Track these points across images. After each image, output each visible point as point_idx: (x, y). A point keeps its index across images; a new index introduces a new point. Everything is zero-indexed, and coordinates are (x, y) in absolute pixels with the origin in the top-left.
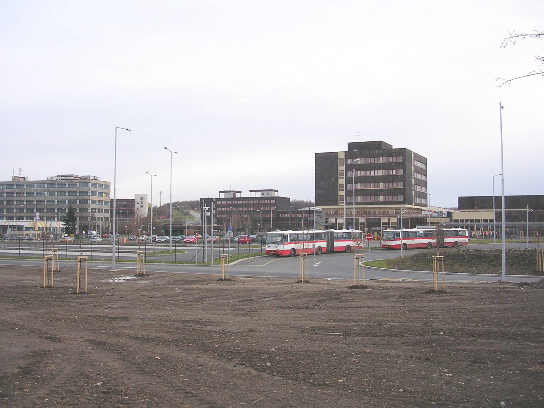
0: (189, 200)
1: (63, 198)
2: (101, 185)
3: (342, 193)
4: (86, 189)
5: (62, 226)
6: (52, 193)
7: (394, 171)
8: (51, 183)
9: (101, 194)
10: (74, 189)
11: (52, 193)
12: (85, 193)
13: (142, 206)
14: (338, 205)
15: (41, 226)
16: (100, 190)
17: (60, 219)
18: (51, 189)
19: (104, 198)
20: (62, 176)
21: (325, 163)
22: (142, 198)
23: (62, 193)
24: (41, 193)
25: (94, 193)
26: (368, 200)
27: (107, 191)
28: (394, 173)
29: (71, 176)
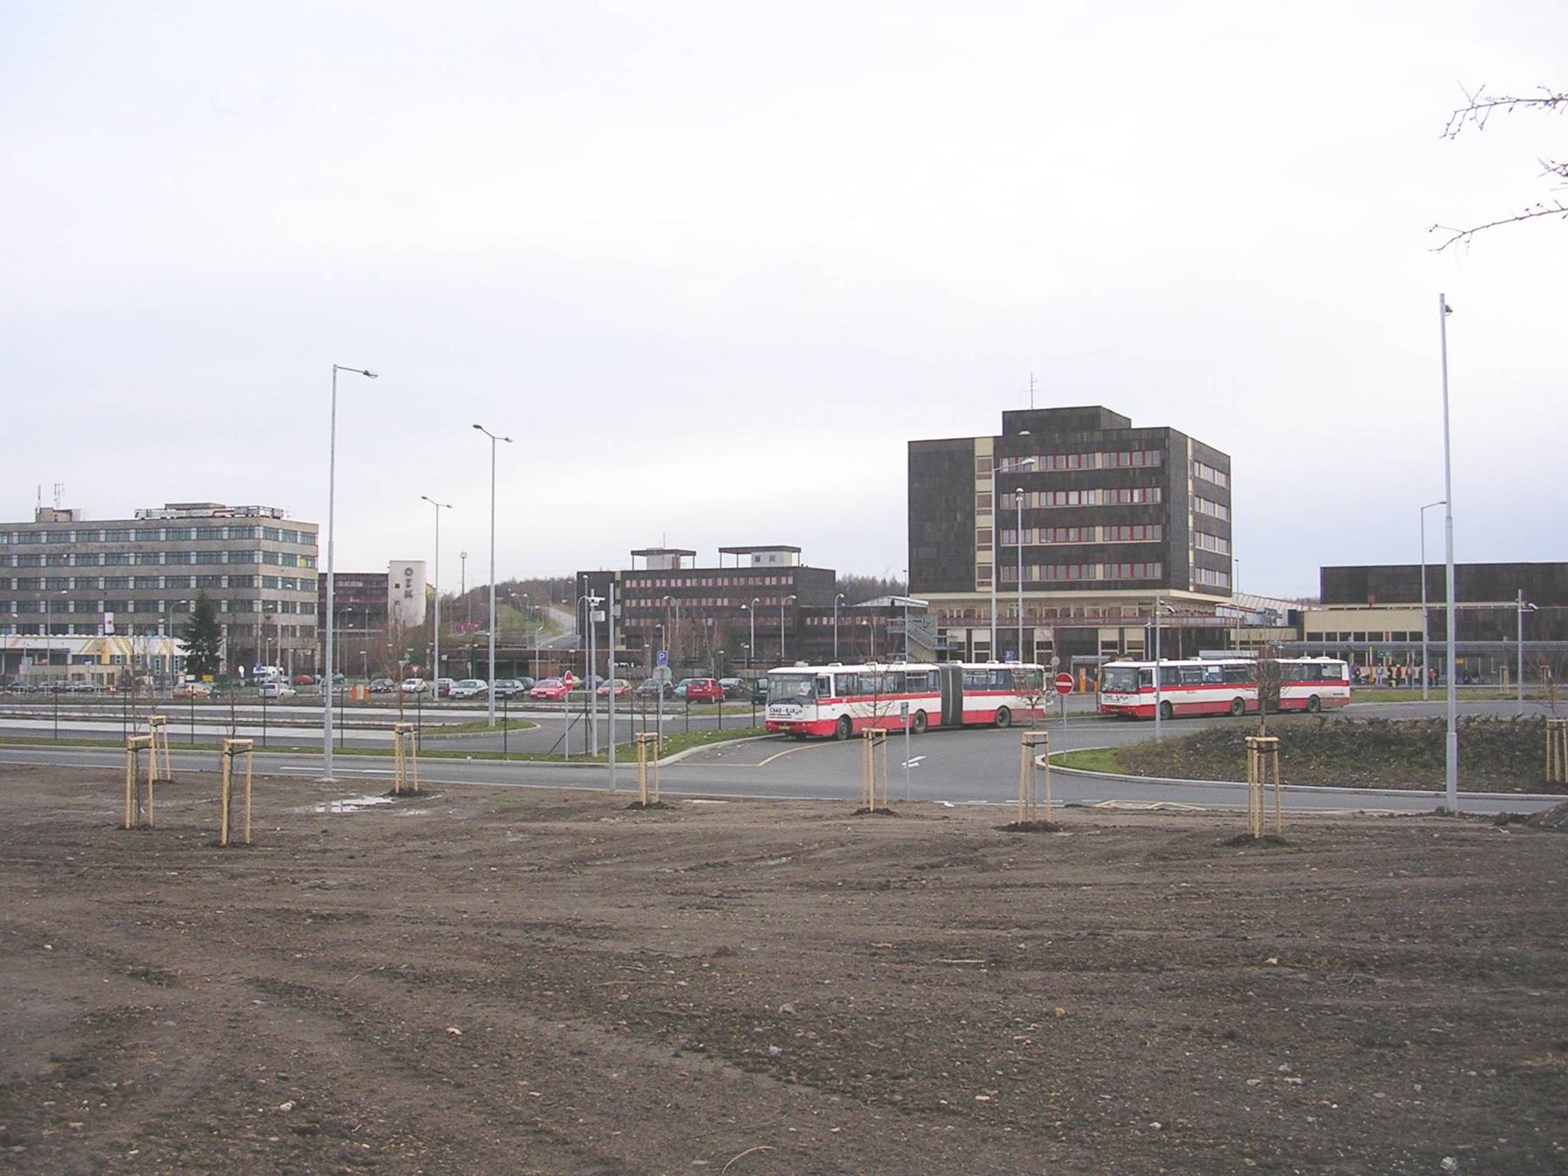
0: (544, 575)
1: (183, 570)
2: (291, 534)
3: (986, 557)
4: (247, 544)
5: (178, 652)
6: (149, 557)
7: (1136, 493)
8: (146, 526)
9: (290, 559)
10: (214, 546)
11: (149, 557)
12: (246, 556)
13: (408, 595)
14: (973, 590)
15: (118, 653)
16: (287, 548)
17: (172, 632)
18: (148, 546)
19: (299, 571)
20: (179, 507)
21: (937, 470)
22: (409, 572)
23: (179, 557)
24: (119, 556)
25: (270, 557)
26: (1061, 578)
27: (308, 551)
28: (1136, 500)
29: (206, 506)
